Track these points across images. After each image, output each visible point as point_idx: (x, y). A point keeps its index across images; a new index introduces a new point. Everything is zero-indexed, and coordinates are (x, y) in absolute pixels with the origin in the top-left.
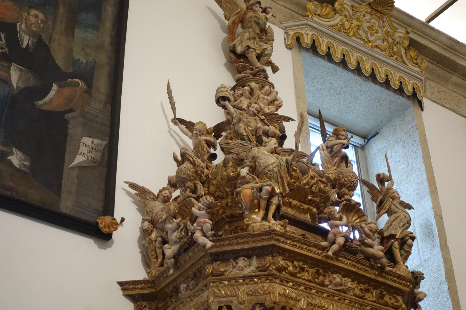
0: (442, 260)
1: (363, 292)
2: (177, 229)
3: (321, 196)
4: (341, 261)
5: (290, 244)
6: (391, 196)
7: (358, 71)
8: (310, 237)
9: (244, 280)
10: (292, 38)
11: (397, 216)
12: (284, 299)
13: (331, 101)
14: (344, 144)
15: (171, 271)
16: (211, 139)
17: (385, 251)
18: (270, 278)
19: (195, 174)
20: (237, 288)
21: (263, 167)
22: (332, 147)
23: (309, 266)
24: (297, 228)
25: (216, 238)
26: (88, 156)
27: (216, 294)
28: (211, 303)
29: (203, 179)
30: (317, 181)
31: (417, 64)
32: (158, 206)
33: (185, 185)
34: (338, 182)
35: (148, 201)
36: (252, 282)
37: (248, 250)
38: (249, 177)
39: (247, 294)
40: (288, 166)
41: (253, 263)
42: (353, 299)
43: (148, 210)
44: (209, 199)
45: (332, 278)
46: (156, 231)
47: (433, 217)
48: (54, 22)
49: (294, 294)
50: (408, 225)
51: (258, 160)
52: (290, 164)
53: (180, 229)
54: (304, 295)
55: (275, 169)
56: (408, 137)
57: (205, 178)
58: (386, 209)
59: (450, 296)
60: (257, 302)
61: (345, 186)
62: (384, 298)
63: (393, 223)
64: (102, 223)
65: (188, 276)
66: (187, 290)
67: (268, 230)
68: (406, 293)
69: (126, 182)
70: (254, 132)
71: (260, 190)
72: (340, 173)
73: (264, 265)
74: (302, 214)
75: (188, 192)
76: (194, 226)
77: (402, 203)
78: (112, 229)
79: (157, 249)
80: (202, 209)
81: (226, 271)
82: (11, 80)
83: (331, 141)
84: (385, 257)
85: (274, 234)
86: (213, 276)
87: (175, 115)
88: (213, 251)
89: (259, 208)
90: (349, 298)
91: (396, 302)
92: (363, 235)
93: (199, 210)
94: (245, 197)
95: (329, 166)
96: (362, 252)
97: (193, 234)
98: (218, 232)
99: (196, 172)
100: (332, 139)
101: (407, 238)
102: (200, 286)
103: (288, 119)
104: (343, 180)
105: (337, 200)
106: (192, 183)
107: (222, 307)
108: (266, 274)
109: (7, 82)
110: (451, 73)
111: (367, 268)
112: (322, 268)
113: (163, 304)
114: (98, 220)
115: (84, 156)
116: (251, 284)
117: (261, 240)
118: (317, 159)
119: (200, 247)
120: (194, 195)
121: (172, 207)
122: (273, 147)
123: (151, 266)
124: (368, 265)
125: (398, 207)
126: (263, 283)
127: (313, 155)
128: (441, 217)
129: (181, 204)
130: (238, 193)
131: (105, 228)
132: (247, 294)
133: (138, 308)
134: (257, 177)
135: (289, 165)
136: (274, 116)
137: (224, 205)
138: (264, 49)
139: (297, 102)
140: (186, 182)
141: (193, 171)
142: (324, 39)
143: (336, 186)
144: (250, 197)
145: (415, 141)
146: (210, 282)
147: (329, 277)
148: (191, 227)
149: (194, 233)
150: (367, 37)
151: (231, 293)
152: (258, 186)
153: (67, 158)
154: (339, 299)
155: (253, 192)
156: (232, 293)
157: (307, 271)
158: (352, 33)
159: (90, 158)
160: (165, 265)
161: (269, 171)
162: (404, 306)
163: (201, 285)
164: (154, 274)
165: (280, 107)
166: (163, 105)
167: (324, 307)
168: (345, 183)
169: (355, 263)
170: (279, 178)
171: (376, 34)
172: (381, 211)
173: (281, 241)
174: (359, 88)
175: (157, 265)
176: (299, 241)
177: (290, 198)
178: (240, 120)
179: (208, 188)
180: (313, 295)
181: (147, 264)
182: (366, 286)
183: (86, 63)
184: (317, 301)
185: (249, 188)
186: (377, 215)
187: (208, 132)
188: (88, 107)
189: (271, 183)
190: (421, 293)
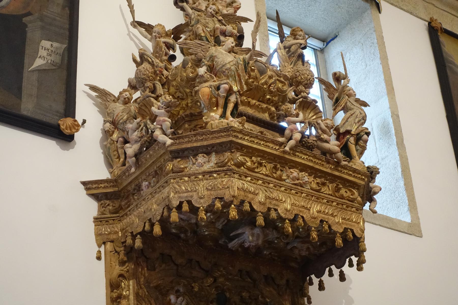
0: (399, 157)
1: (320, 185)
2: (138, 129)
3: (279, 95)
4: (298, 156)
5: (248, 140)
6: (347, 94)
8: (268, 134)
9: (204, 176)
11: (353, 112)
12: (242, 193)
13: (290, 5)
14: (301, 44)
15: (133, 170)
16: (170, 41)
17: (341, 146)
18: (229, 173)
19: (154, 74)
20: (197, 183)
21: (220, 66)
22: (290, 47)
23: (267, 162)
24: (255, 126)
25: (174, 135)
26: (48, 59)
27: (177, 190)
28: (172, 199)
29: (163, 81)
30: (275, 80)
32: (119, 108)
33: (144, 85)
34: (295, 80)
35: (109, 103)
36: (211, 178)
37: (207, 146)
38: (207, 76)
39: (207, 189)
40: (245, 65)
41: (212, 159)
42: (310, 193)
43: (109, 112)
44: (168, 97)
45: (289, 173)
46: (117, 132)
47: (390, 117)
49: (252, 188)
50: (363, 121)
51: (216, 59)
52: (247, 63)
54: (262, 189)
55: (232, 67)
56: (366, 39)
57: (165, 80)
58: (342, 106)
59: (406, 192)
60: (216, 197)
61: (301, 84)
62: (340, 192)
63: (349, 119)
64: (63, 125)
65: (149, 174)
66: (148, 188)
67: (226, 126)
68: (362, 187)
69: (86, 85)
70: (212, 33)
71: (218, 88)
72: (296, 71)
74: (261, 113)
75: (147, 92)
76: (154, 125)
77: (358, 100)
79: (118, 149)
80: (161, 108)
81: (186, 168)
83: (289, 41)
84: (341, 152)
85: (232, 130)
86: (173, 173)
87: (134, 18)
88: (173, 148)
89: (217, 106)
90: (306, 191)
91: (352, 195)
92: (319, 131)
93: (159, 109)
94: (203, 96)
95: (286, 64)
96: (318, 148)
97: (153, 132)
98: (178, 131)
99: (155, 72)
101: (362, 134)
103: (246, 20)
104: (300, 78)
105: (294, 98)
106: (151, 83)
107: (183, 201)
108: (225, 169)
111: (323, 163)
112: (279, 163)
113: (126, 201)
114: (60, 122)
115: (43, 59)
116: (210, 179)
117: (220, 136)
118: (275, 61)
119: (160, 145)
120: (153, 95)
121: (133, 108)
122: (230, 46)
123: (113, 167)
124: (324, 159)
125: (354, 104)
126: (222, 178)
127: (271, 56)
128: (398, 116)
129: (141, 104)
130: (197, 92)
131: (67, 129)
132: (207, 189)
133: (101, 207)
134: (215, 76)
135: (246, 64)
136: (231, 17)
137: (184, 106)
139: (256, 5)
140: (146, 83)
141: (152, 71)
143: (293, 84)
145: (373, 43)
146: (171, 178)
148: (151, 126)
149: (154, 132)
151: (191, 188)
152: (216, 85)
153: (26, 61)
154: (297, 193)
155: (211, 91)
156: (192, 189)
157: (265, 166)
159: (49, 61)
160: (127, 165)
161: (226, 69)
162: (359, 199)
163: (162, 182)
164: (116, 173)
165: (238, 8)
166: (122, 8)
167: (282, 201)
168: (302, 81)
169: (311, 158)
170: (237, 77)
172: (338, 108)
173: (239, 137)
175: (119, 165)
176: (256, 137)
177: (248, 97)
178: (198, 21)
179: (169, 89)
180: (271, 189)
181: (109, 164)
182: (323, 179)
184: (275, 194)
185: (207, 87)
186: (333, 112)
187: (167, 35)
188: (46, 11)
190: (376, 187)
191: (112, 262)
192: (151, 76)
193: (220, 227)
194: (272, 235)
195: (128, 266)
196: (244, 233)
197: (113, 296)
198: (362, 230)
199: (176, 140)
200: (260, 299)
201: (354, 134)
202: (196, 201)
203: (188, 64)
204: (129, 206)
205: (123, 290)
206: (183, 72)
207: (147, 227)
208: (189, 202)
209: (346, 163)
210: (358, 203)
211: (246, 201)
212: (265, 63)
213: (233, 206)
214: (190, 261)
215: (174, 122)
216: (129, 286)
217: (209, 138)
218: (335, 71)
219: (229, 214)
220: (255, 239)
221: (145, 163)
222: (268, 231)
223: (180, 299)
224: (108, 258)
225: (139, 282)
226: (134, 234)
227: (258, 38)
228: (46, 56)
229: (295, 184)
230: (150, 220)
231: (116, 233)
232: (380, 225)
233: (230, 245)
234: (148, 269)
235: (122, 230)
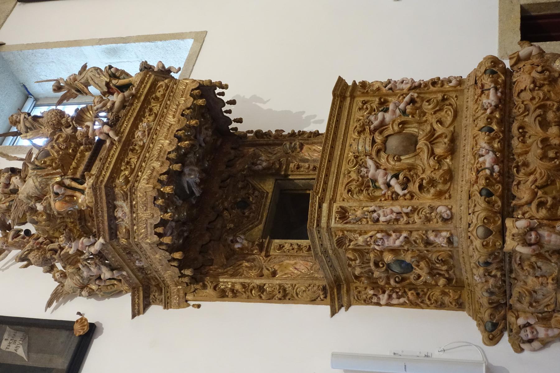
2: (88, 267)
3: (70, 141)
4: (124, 130)
9: (134, 212)
12: (152, 181)
14: (25, 117)
15: (124, 273)
16: (11, 233)
17: (120, 92)
19: (40, 249)
21: (36, 190)
24: (95, 165)
25: (96, 236)
30: (56, 143)
33: (49, 259)
37: (108, 207)
39: (145, 211)
43: (72, 291)
44: (61, 239)
46: (91, 285)
51: (30, 194)
53: (88, 264)
57: (48, 240)
61: (60, 120)
64: (80, 332)
66: (141, 261)
69: (46, 310)
71: (57, 194)
72: (48, 124)
73: (121, 195)
75: (55, 256)
77: (80, 73)
78: (86, 323)
80: (71, 246)
81: (126, 227)
83: (21, 128)
84: (124, 92)
85: (96, 185)
86: (129, 239)
88: (107, 237)
89: (73, 196)
91: (162, 87)
92: (104, 109)
93: (71, 248)
95: (41, 132)
96: (119, 111)
99: (38, 249)
100: (19, 127)
101: (110, 72)
102: (137, 250)
104: (54, 122)
111: (132, 109)
113: (152, 281)
114: (77, 335)
118: (41, 142)
119: (104, 249)
120: (59, 252)
124: (129, 108)
126: (137, 197)
127: (35, 145)
128: (101, 39)
130: (59, 213)
131: (84, 329)
132: (145, 211)
134: (46, 196)
137: (72, 225)
144: (62, 203)
148: (86, 256)
153: (19, 363)
154: (156, 134)
155: (59, 200)
159: (21, 342)
160: (120, 278)
161: (40, 186)
162: (166, 81)
164: (127, 288)
168: (57, 120)
170: (48, 177)
175: (120, 285)
176: (104, 164)
181: (119, 293)
182: (147, 110)
184: (156, 153)
187: (6, 236)
189: (51, 185)
190: (158, 65)
191: (203, 295)
192: (41, 252)
193: (181, 202)
194: (191, 158)
195: (207, 282)
196: (187, 182)
197: (231, 296)
198: (193, 82)
199: (100, 234)
200: (245, 173)
201: (110, 79)
202: (155, 220)
203: (34, 219)
204: (156, 278)
205: (227, 287)
206: (41, 224)
207: (175, 264)
208: (156, 226)
209: (134, 88)
210: (170, 82)
211: (159, 178)
212: (39, 150)
213: (162, 189)
214: (208, 229)
215: (85, 235)
216: (224, 282)
217: (101, 206)
218: (52, 90)
219: (168, 194)
220: (193, 173)
221: (119, 262)
222: (188, 162)
223: (238, 239)
224: (199, 298)
225: (221, 273)
226: (180, 275)
227: (13, 156)
228: (16, 345)
229: (148, 135)
230: (169, 261)
231: (178, 290)
232: (194, 66)
233: (197, 194)
234: (212, 265)
235: (176, 285)
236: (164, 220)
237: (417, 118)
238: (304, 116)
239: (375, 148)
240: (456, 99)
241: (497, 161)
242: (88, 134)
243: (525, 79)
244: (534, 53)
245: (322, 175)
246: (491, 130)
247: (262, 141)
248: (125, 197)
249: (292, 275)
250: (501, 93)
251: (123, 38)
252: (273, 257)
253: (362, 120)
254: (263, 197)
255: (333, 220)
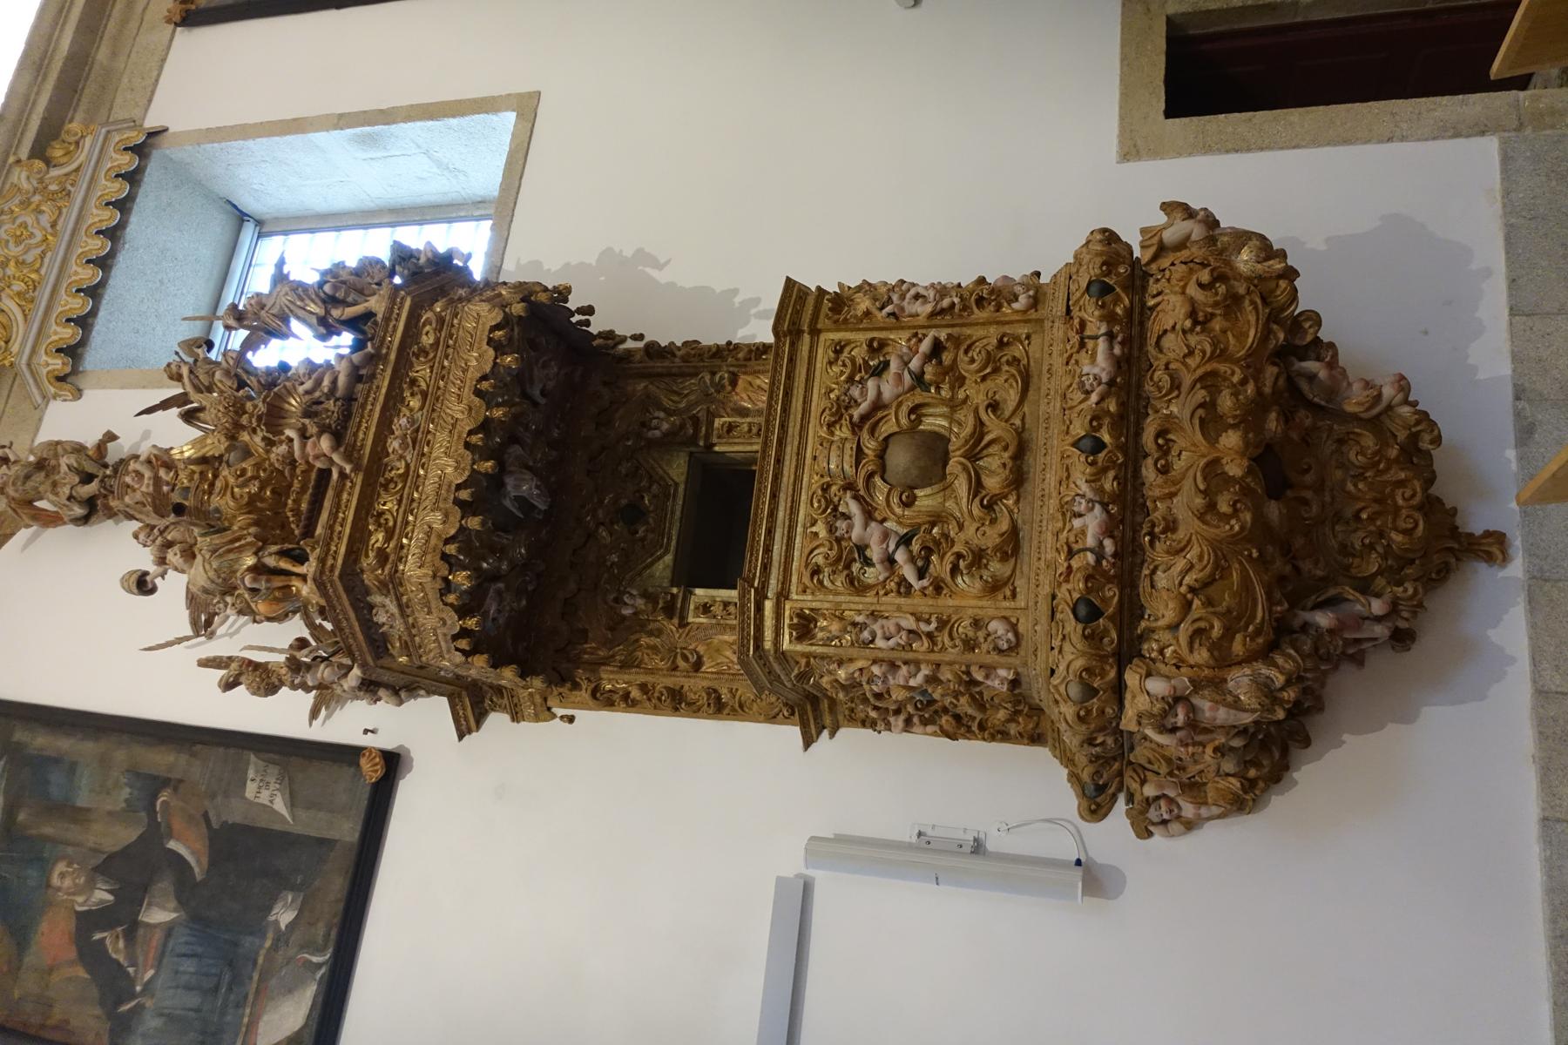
7: (104, 263)
9: (408, 616)
10: (61, 389)
31: (77, 143)
48: (68, 843)
69: (311, 724)
71: (254, 591)
82: (165, 923)
85: (321, 577)
101: (322, 295)
109: (169, 929)
110: (93, 63)
128: (341, 116)
136: (157, 502)
138: (70, 469)
142: (52, 331)
147: (393, 461)
150: (37, 245)
153: (277, 827)
158: (33, 276)
159: (278, 786)
161: (219, 577)
171: (30, 228)
174: (141, 250)
183: (131, 787)
184: (429, 487)
201: (326, 308)
229: (414, 443)
232: (521, 178)
234: (586, 642)
236: (466, 629)
237: (946, 393)
238: (737, 300)
239: (863, 473)
240: (1027, 342)
241: (1108, 531)
242: (293, 456)
243: (1175, 306)
244: (1194, 237)
245: (760, 535)
246: (1099, 445)
247: (659, 366)
248: (384, 587)
249: (729, 668)
250: (1122, 343)
251: (381, 111)
252: (695, 627)
253: (836, 391)
254: (667, 496)
255: (787, 637)
